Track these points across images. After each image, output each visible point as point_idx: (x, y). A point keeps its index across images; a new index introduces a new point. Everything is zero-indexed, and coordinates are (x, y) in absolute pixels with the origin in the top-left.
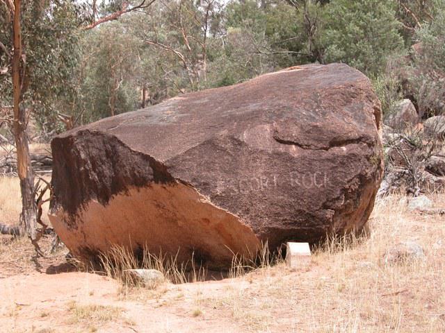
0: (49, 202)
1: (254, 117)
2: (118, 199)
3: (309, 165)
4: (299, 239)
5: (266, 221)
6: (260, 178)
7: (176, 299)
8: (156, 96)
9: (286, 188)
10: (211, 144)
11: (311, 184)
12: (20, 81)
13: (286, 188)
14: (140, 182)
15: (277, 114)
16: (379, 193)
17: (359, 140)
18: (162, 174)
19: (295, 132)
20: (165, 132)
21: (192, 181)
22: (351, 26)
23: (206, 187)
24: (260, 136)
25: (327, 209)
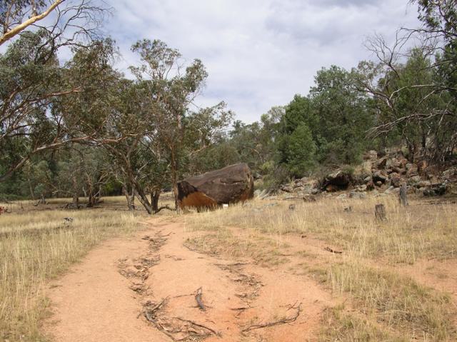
0: (159, 208)
1: (217, 177)
2: (189, 196)
3: (228, 187)
4: (226, 203)
5: (218, 200)
6: (217, 190)
7: (285, 261)
8: (291, 130)
9: (223, 192)
10: (206, 183)
11: (228, 191)
12: (150, 229)
13: (223, 192)
14: (192, 192)
15: (221, 176)
16: (20, 202)
17: (241, 181)
18: (196, 190)
19: (225, 179)
20: (346, 138)
21: (398, 180)
22: (296, 144)
23: (205, 192)
24: (218, 181)
25: (139, 194)
